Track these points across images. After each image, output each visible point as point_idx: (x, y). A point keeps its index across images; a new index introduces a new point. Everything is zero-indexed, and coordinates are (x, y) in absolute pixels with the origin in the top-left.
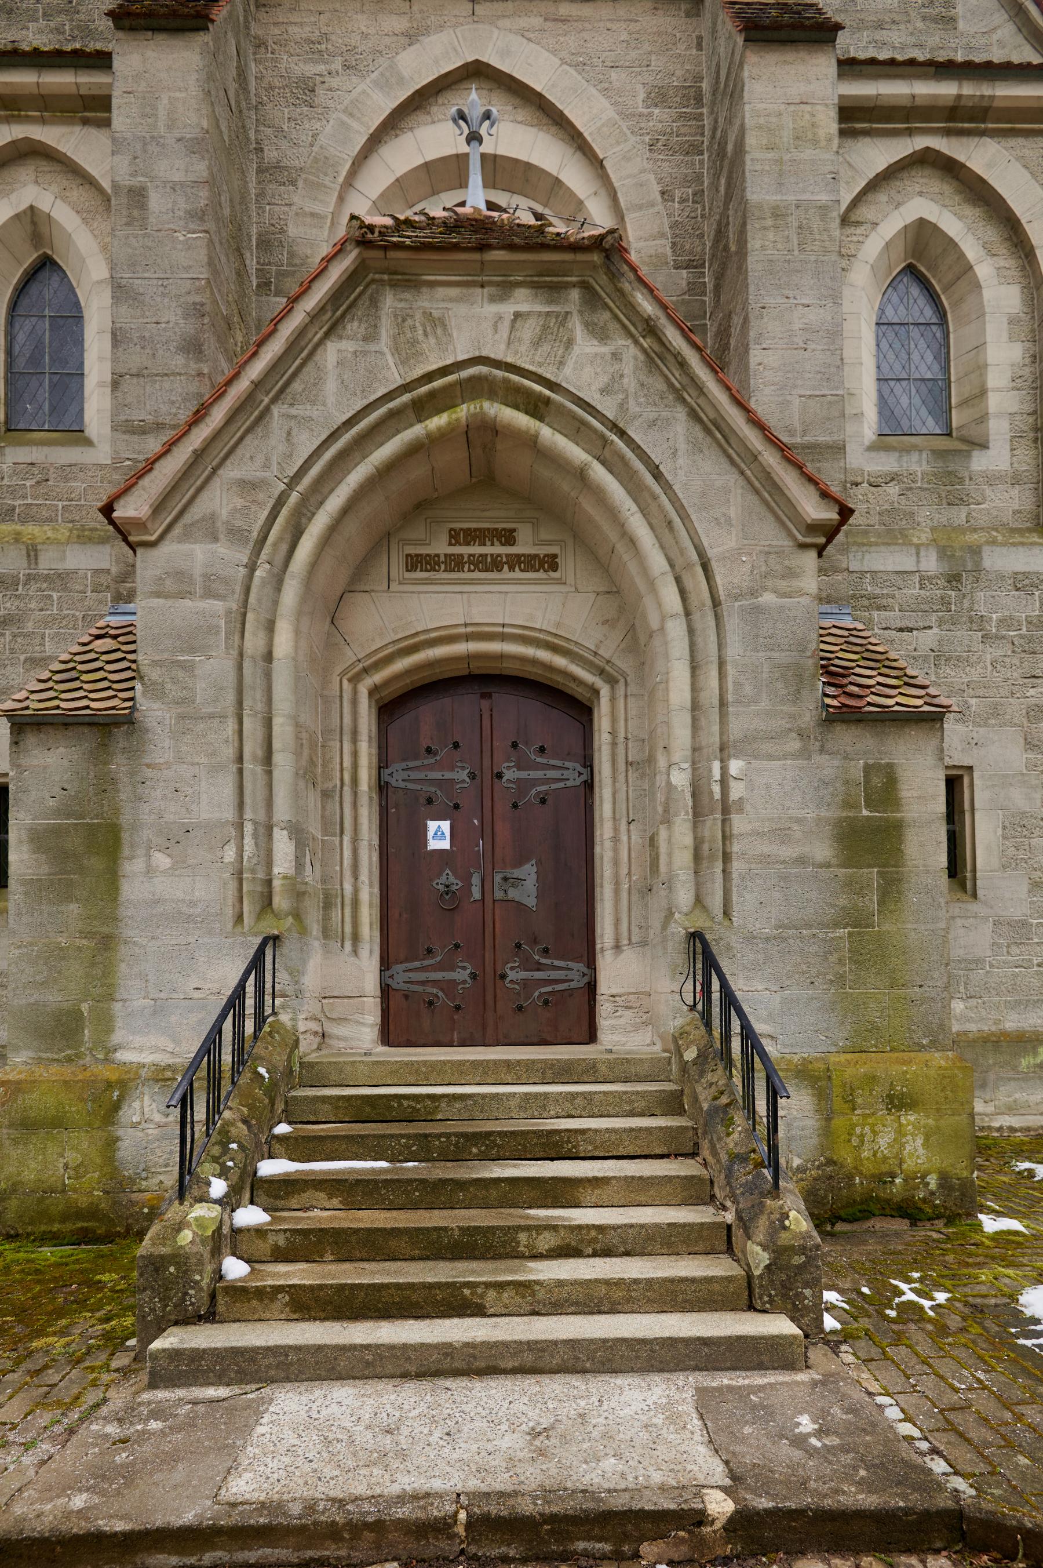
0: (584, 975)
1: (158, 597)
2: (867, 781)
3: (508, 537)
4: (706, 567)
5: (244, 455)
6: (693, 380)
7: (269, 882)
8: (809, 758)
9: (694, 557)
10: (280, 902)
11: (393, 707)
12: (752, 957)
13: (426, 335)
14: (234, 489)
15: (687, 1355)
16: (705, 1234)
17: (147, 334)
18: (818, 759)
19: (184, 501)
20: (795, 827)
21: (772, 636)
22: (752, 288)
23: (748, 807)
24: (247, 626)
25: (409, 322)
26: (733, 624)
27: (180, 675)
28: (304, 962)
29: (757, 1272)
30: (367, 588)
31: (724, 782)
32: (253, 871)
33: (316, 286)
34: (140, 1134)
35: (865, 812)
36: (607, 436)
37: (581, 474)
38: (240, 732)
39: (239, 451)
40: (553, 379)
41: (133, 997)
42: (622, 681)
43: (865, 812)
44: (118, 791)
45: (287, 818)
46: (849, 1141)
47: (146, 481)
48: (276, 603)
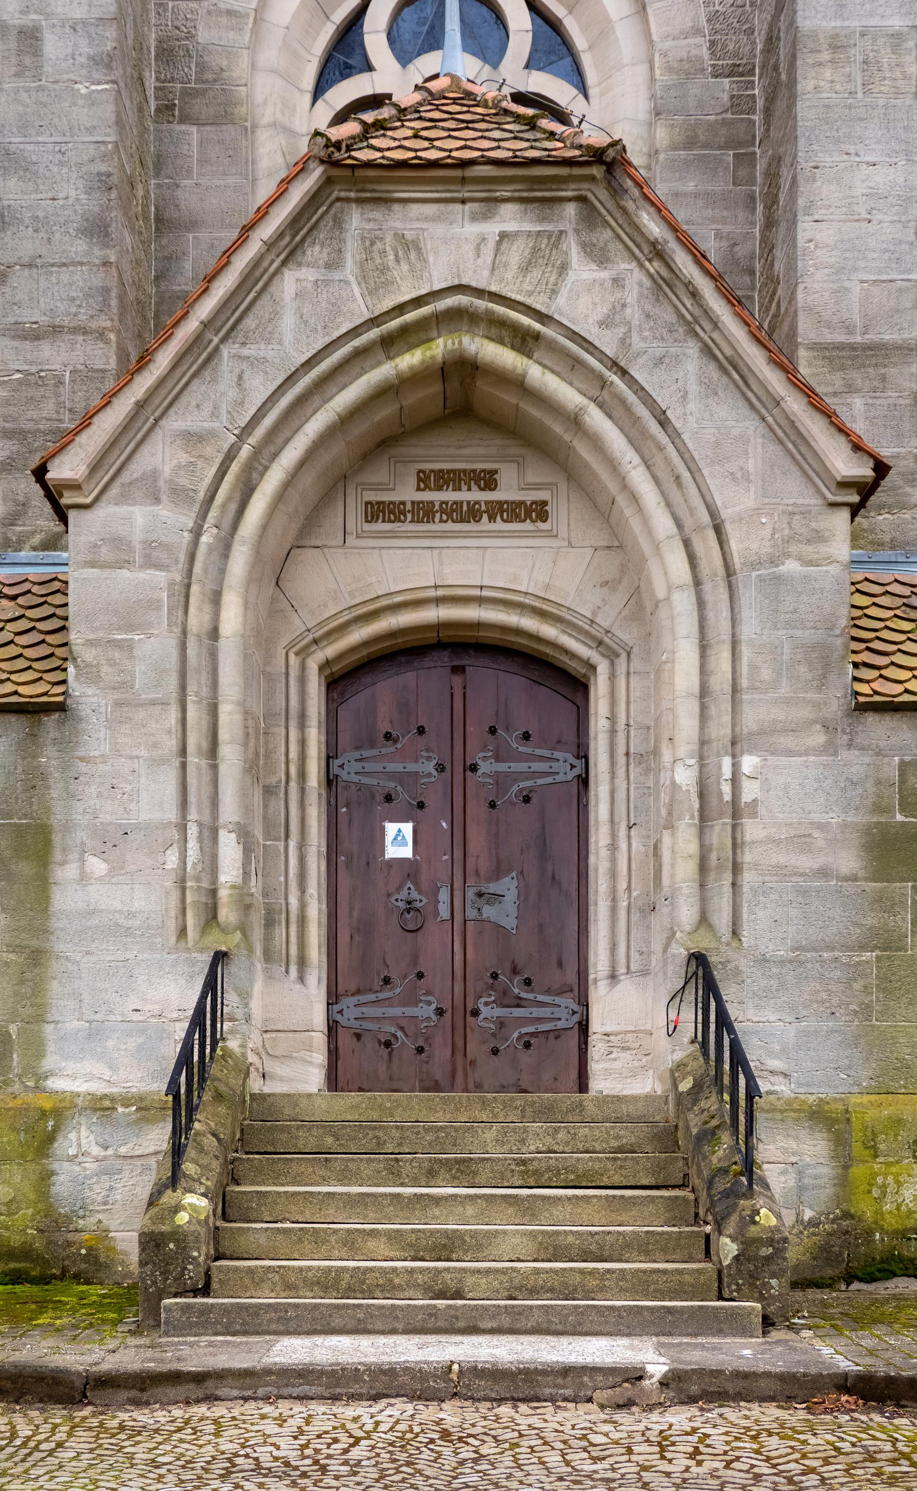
0: (574, 1013)
1: (93, 567)
2: (902, 781)
3: (488, 481)
4: (718, 529)
5: (189, 403)
6: (707, 313)
7: (214, 892)
8: (835, 754)
9: (705, 518)
10: (227, 914)
11: (342, 680)
12: (763, 983)
13: (397, 261)
14: (178, 442)
15: (652, 1322)
16: (683, 1243)
17: (41, 214)
18: (845, 755)
19: (123, 458)
20: (816, 834)
21: (795, 611)
22: (802, 142)
23: (762, 810)
24: (192, 600)
25: (379, 245)
26: (748, 596)
27: (117, 655)
28: (251, 982)
29: (726, 1263)
30: (313, 542)
31: (735, 781)
32: (198, 879)
33: (274, 211)
34: (77, 1168)
35: (899, 818)
36: (608, 375)
37: (575, 421)
38: (183, 721)
39: (184, 399)
40: (544, 310)
41: (66, 1018)
42: (624, 655)
43: (899, 818)
44: (49, 788)
45: (236, 819)
46: (870, 1192)
47: (83, 438)
48: (222, 571)
